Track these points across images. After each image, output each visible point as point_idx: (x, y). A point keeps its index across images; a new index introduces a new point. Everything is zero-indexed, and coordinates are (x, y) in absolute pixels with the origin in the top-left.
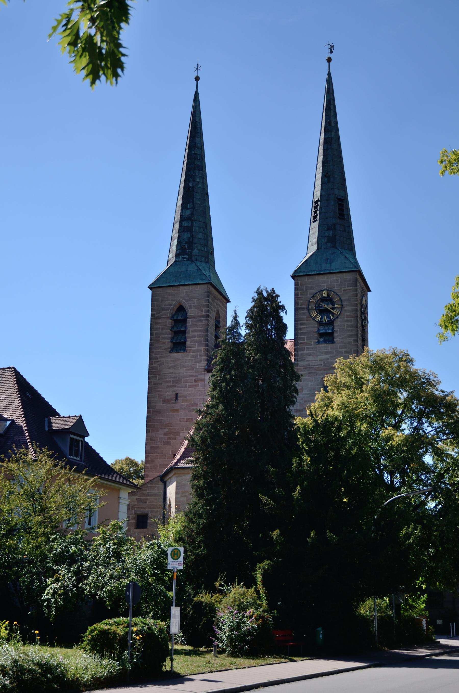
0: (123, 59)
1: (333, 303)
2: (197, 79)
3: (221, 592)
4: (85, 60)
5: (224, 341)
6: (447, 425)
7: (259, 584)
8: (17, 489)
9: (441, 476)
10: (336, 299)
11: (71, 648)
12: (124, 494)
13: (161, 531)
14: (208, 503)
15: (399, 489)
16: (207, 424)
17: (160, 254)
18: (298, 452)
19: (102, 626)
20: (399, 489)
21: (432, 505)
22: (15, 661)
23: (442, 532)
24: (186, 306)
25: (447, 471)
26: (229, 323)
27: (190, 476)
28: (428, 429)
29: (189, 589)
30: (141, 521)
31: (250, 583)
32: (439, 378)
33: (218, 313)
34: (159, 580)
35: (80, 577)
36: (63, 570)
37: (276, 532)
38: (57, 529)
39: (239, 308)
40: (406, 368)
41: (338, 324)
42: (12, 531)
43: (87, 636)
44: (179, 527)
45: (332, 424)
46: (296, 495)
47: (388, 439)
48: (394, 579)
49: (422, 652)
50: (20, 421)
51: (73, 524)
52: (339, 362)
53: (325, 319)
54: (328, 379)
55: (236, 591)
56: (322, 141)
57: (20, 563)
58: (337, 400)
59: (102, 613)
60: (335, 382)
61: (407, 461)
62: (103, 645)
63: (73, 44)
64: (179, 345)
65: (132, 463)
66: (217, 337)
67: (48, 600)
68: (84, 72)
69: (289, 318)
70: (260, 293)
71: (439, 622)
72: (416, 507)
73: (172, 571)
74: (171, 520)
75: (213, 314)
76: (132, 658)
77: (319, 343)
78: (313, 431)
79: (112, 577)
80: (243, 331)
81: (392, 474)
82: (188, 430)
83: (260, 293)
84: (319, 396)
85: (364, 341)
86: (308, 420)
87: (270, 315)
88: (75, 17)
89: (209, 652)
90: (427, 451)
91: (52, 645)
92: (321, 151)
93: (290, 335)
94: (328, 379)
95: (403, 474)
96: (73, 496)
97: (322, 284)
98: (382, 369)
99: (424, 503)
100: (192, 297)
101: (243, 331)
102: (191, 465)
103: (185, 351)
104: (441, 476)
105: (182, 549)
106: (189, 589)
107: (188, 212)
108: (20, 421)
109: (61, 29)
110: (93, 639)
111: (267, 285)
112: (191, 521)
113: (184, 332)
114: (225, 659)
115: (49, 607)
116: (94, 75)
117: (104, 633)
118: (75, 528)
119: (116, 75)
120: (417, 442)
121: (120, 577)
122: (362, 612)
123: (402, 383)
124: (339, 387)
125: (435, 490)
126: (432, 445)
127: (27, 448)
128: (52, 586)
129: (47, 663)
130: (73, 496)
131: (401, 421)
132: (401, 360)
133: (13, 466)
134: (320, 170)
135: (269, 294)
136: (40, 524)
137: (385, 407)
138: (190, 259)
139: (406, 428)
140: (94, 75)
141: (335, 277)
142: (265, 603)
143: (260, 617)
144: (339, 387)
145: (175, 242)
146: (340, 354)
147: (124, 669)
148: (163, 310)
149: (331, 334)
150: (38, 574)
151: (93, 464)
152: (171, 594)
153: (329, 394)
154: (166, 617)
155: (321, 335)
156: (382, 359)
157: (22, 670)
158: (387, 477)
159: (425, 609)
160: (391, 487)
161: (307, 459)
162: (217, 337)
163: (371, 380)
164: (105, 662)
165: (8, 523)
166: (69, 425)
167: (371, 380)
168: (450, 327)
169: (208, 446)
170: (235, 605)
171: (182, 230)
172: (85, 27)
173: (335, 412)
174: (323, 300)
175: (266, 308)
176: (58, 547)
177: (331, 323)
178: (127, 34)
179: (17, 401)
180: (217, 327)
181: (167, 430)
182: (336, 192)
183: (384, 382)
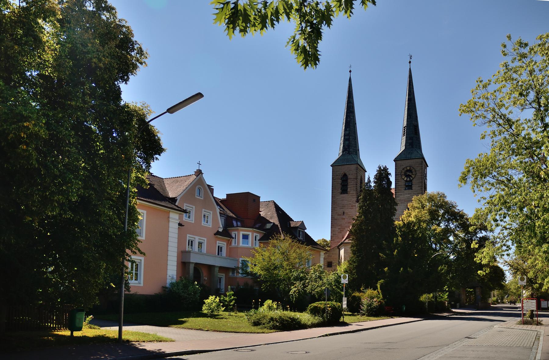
0: (319, 57)
1: (412, 172)
2: (350, 71)
3: (363, 292)
4: (302, 58)
5: (364, 189)
6: (460, 224)
7: (379, 289)
8: (277, 251)
9: (456, 245)
10: (413, 170)
11: (302, 312)
12: (322, 253)
13: (338, 268)
14: (358, 257)
15: (439, 250)
16: (357, 225)
17: (335, 151)
18: (397, 236)
19: (315, 304)
20: (439, 250)
21: (452, 257)
22: (280, 317)
23: (456, 268)
24: (347, 174)
25: (459, 243)
26: (366, 181)
27: (350, 246)
28: (452, 226)
29: (350, 291)
30: (329, 265)
31: (375, 288)
32: (457, 204)
33: (361, 177)
34: (338, 288)
35: (305, 286)
36: (298, 283)
37: (386, 269)
38: (293, 266)
39: (371, 174)
40: (443, 200)
41: (414, 181)
42: (276, 268)
43: (309, 308)
44: (345, 266)
45: (411, 224)
46: (395, 253)
47: (435, 230)
48: (435, 285)
49: (445, 314)
50: (277, 223)
51: (301, 265)
52: (414, 198)
53: (408, 179)
54: (409, 205)
55: (369, 292)
56: (407, 99)
57: (280, 281)
58: (413, 214)
59: (314, 300)
60: (412, 206)
61: (442, 239)
62: (315, 311)
63: (297, 50)
64: (344, 190)
65: (325, 241)
66: (361, 187)
67: (292, 295)
68: (301, 63)
69: (392, 179)
70: (380, 168)
71: (453, 303)
72: (445, 258)
73: (343, 284)
74: (342, 264)
75: (359, 177)
76: (327, 316)
77: (405, 189)
78: (403, 227)
79: (318, 286)
80: (373, 184)
81: (436, 245)
82: (349, 227)
83: (380, 168)
84: (405, 212)
85: (425, 188)
86: (401, 223)
87: (384, 177)
88: (297, 38)
89: (358, 315)
90: (451, 235)
91: (295, 311)
92: (407, 104)
93: (393, 186)
94: (409, 205)
95: (441, 244)
96: (301, 254)
97: (407, 164)
98: (433, 200)
99: (449, 256)
100: (350, 170)
101: (373, 184)
102: (350, 241)
103: (347, 193)
104: (456, 245)
105: (347, 275)
106: (350, 291)
107: (347, 132)
108: (277, 223)
109: (291, 43)
110: (311, 309)
111: (383, 164)
112: (350, 264)
113: (347, 185)
114: (365, 317)
115: (293, 297)
116: (306, 64)
117: (316, 307)
118: (302, 267)
119: (316, 64)
120: (447, 231)
121: (321, 286)
122: (422, 299)
123: (441, 206)
124: (414, 208)
125: (454, 251)
126: (453, 232)
127: (281, 234)
128: (293, 289)
129: (293, 318)
130: (301, 254)
131: (440, 223)
132: (441, 197)
133: (275, 241)
134: (406, 113)
135: (384, 168)
136: (287, 265)
137: (433, 215)
138: (349, 153)
139: (443, 225)
140: (306, 64)
141: (412, 161)
142: (381, 296)
143: (380, 301)
144: (414, 208)
145: (342, 146)
146: (415, 194)
147: (324, 320)
148: (337, 175)
149: (411, 186)
150: (288, 284)
151: (309, 241)
152: (343, 293)
153: (410, 211)
154: (341, 301)
155: (407, 186)
156: (433, 196)
157: (283, 320)
158: (434, 246)
159: (447, 298)
160: (435, 250)
161: (400, 238)
162: (361, 187)
163: (428, 205)
164: (316, 318)
165: (274, 264)
166: (298, 225)
167: (428, 205)
168: (463, 181)
169: (357, 233)
170: (369, 296)
171: (345, 140)
172: (302, 42)
173: (412, 219)
174: (407, 171)
175: (382, 174)
176: (295, 274)
177: (411, 181)
178: (321, 45)
179: (275, 215)
180: (361, 183)
181: (340, 227)
182: (413, 122)
183: (433, 206)
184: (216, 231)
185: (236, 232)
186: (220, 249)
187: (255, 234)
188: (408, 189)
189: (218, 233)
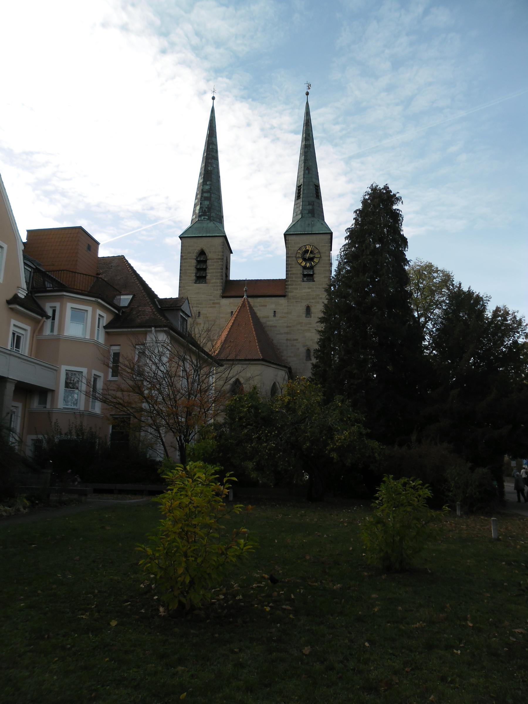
24: (207, 251)
53: (308, 265)
75: (225, 259)
107: (207, 187)
148: (189, 253)
149: (312, 275)
155: (305, 276)
177: (312, 268)
184: (10, 296)
185: (57, 305)
186: (17, 341)
187: (99, 312)
188: (308, 281)
189: (15, 300)
